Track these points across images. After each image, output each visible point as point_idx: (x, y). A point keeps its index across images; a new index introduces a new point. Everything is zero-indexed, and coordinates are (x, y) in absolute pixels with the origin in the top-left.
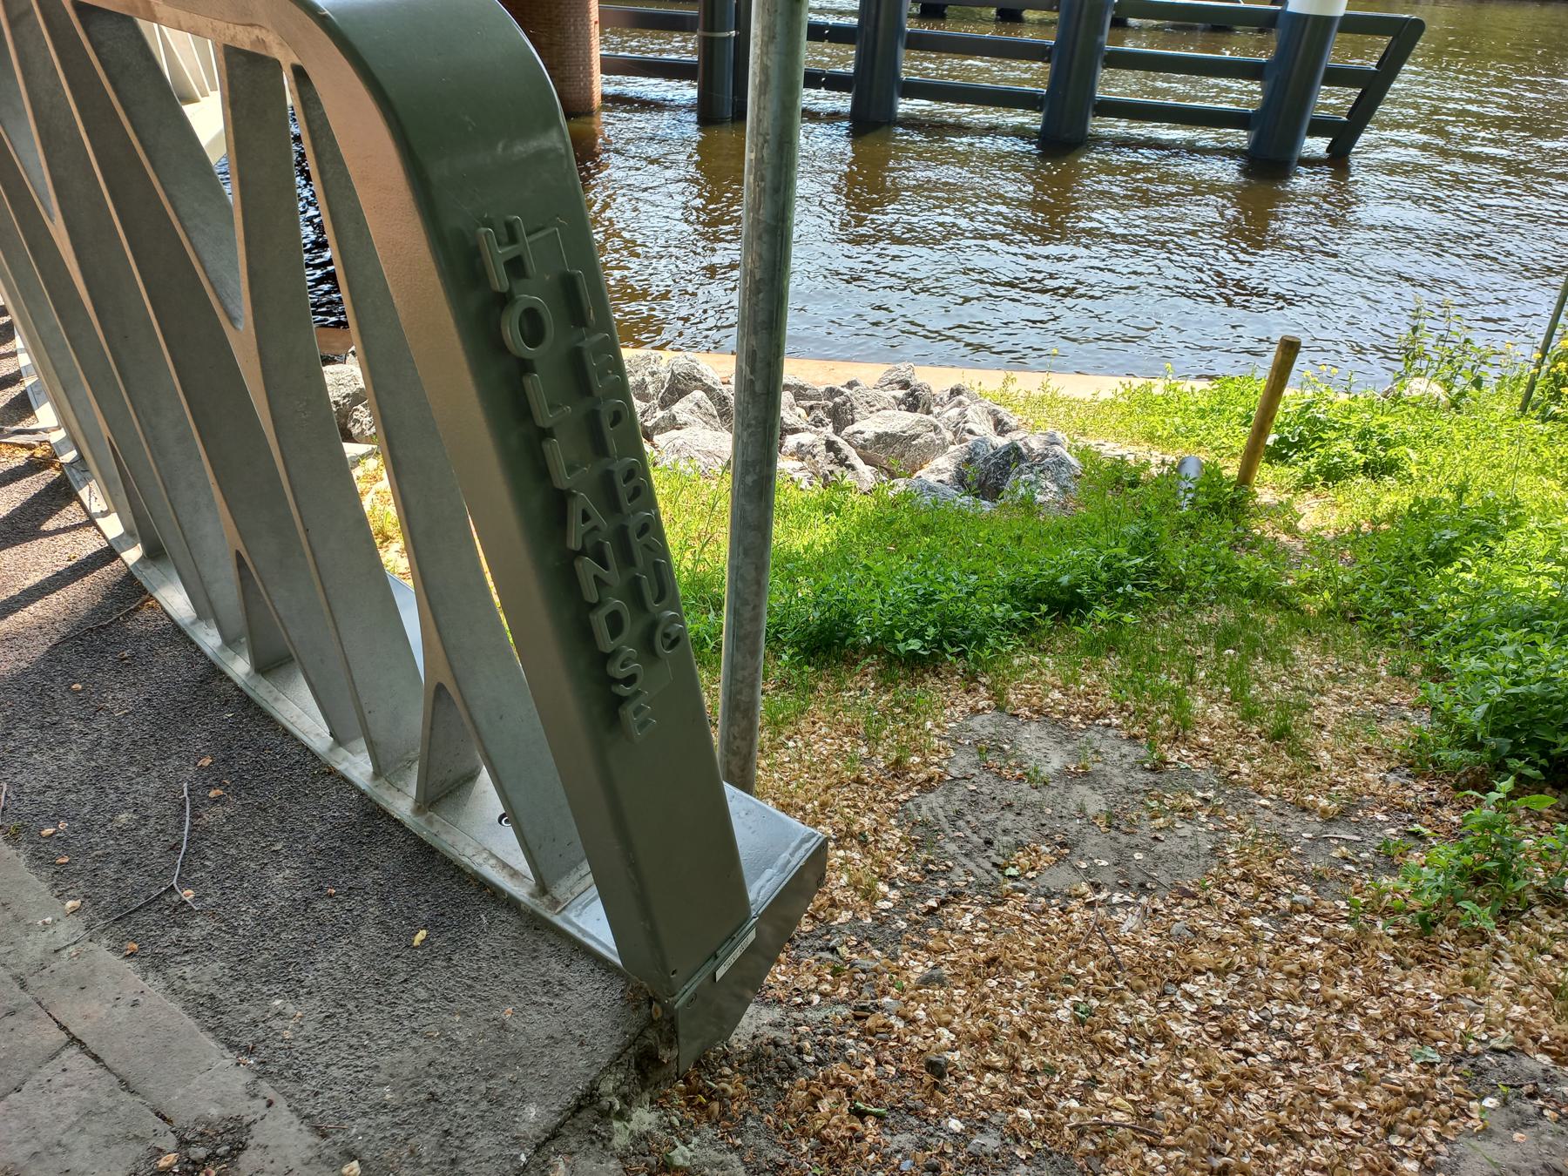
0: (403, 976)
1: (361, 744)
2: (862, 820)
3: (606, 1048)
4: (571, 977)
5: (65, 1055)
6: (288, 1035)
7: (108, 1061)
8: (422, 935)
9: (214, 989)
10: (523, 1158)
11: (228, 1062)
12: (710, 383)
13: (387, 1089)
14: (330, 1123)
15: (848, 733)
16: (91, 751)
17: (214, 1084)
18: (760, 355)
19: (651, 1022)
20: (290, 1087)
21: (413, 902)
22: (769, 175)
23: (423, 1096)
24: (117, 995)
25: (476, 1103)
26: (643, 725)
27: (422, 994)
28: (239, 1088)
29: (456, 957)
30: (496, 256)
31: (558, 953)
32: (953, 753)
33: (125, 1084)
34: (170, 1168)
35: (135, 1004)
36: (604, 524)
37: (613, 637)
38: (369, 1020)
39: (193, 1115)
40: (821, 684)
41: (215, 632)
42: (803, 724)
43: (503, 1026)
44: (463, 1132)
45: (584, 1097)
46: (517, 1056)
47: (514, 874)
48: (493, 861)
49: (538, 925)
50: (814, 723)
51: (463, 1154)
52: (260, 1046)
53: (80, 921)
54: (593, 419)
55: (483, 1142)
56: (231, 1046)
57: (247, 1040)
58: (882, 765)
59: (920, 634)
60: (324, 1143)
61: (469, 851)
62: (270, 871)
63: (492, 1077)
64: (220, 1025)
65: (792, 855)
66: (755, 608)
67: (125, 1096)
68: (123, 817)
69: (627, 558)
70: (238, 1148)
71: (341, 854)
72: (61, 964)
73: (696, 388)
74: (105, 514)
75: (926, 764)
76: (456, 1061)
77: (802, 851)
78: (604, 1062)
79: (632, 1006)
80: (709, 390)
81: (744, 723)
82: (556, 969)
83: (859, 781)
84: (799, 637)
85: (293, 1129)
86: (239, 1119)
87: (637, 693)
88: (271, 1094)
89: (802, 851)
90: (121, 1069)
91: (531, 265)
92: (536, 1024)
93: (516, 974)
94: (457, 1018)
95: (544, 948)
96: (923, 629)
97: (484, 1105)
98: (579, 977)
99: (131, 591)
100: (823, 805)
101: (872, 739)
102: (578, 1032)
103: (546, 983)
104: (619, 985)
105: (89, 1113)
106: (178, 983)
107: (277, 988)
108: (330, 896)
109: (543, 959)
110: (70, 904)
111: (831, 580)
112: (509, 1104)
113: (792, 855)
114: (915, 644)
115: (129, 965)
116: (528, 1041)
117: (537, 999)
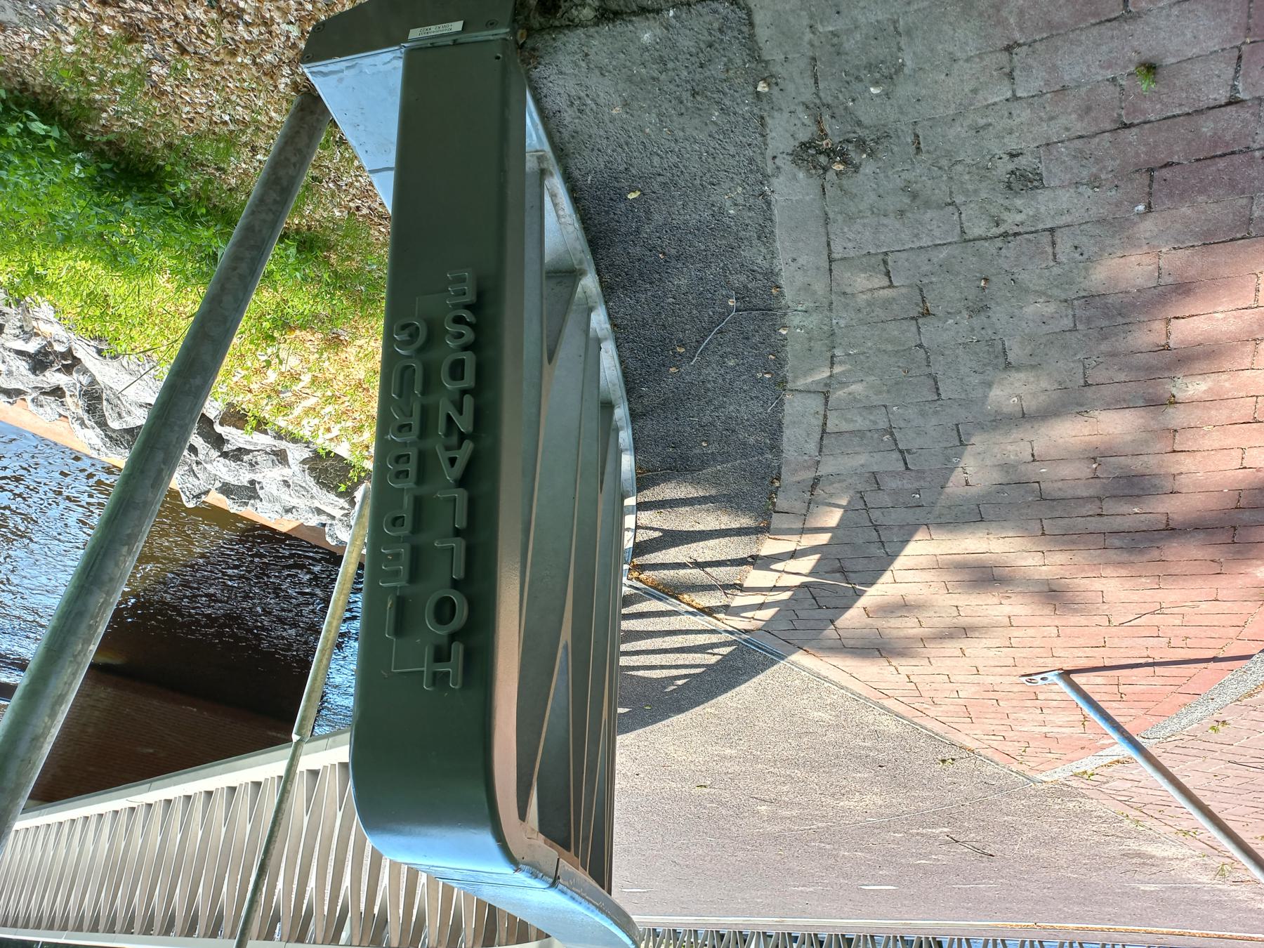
0: (660, 179)
1: (592, 334)
2: (203, 17)
3: (573, 39)
4: (562, 102)
5: (839, 256)
6: (740, 189)
7: (824, 239)
8: (632, 196)
9: (755, 242)
10: (671, 13)
11: (776, 196)
12: (98, 430)
13: (714, 118)
14: (756, 122)
15: (164, 93)
16: (722, 406)
17: (791, 189)
18: (148, 482)
19: (530, 31)
20: (759, 159)
21: (623, 219)
22: (83, 628)
23: (699, 98)
24: (795, 266)
25: (674, 70)
26: (463, 280)
27: (656, 160)
28: (782, 178)
29: (621, 168)
30: (454, 668)
31: (560, 124)
32: (60, 9)
33: (827, 220)
34: (840, 162)
35: (794, 260)
36: (439, 449)
37: (462, 361)
38: (694, 166)
39: (811, 181)
40: (159, 145)
41: (620, 440)
42: (204, 127)
43: (626, 104)
44: (693, 59)
45: (609, 19)
46: (630, 79)
47: (553, 196)
48: (561, 213)
49: (560, 152)
50: (191, 120)
51: (702, 46)
52: (757, 193)
53: (786, 321)
54: (417, 526)
55: (687, 43)
56: (769, 203)
57: (760, 201)
58: (147, 46)
59: (26, 132)
60: (765, 114)
61: (571, 229)
62: (684, 289)
63: (654, 79)
64: (766, 219)
65: (342, 71)
66: (235, 269)
67: (831, 215)
68: (731, 363)
69: (427, 415)
70: (805, 146)
71: (641, 275)
72: (809, 304)
73: (114, 431)
74: (628, 529)
75: (99, 19)
76: (667, 105)
77: (332, 68)
78: (580, 31)
79: (537, 54)
80: (102, 424)
81: (282, 173)
82: (568, 116)
83: (183, 51)
84: (155, 195)
85: (774, 134)
86: (794, 162)
87: (456, 306)
88: (770, 162)
89: (332, 68)
90: (822, 230)
91: (428, 653)
92: (604, 90)
93: (594, 131)
94: (647, 130)
95: (566, 135)
96: (19, 135)
97: (670, 65)
98: (557, 101)
99: (644, 480)
100: (233, 53)
101: (140, 74)
102: (583, 64)
103: (581, 111)
104: (535, 74)
105: (850, 219)
106: (768, 257)
107: (726, 220)
108: (664, 254)
109: (571, 127)
110: (784, 332)
111: (94, 227)
112: (656, 54)
113: (342, 71)
114: (38, 127)
115: (782, 282)
116: (617, 84)
117: (594, 107)
